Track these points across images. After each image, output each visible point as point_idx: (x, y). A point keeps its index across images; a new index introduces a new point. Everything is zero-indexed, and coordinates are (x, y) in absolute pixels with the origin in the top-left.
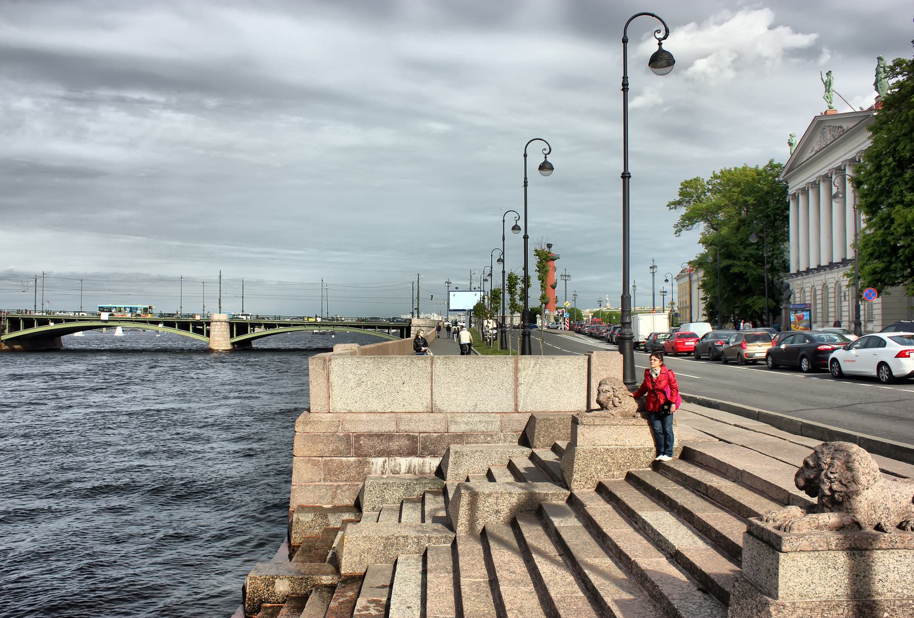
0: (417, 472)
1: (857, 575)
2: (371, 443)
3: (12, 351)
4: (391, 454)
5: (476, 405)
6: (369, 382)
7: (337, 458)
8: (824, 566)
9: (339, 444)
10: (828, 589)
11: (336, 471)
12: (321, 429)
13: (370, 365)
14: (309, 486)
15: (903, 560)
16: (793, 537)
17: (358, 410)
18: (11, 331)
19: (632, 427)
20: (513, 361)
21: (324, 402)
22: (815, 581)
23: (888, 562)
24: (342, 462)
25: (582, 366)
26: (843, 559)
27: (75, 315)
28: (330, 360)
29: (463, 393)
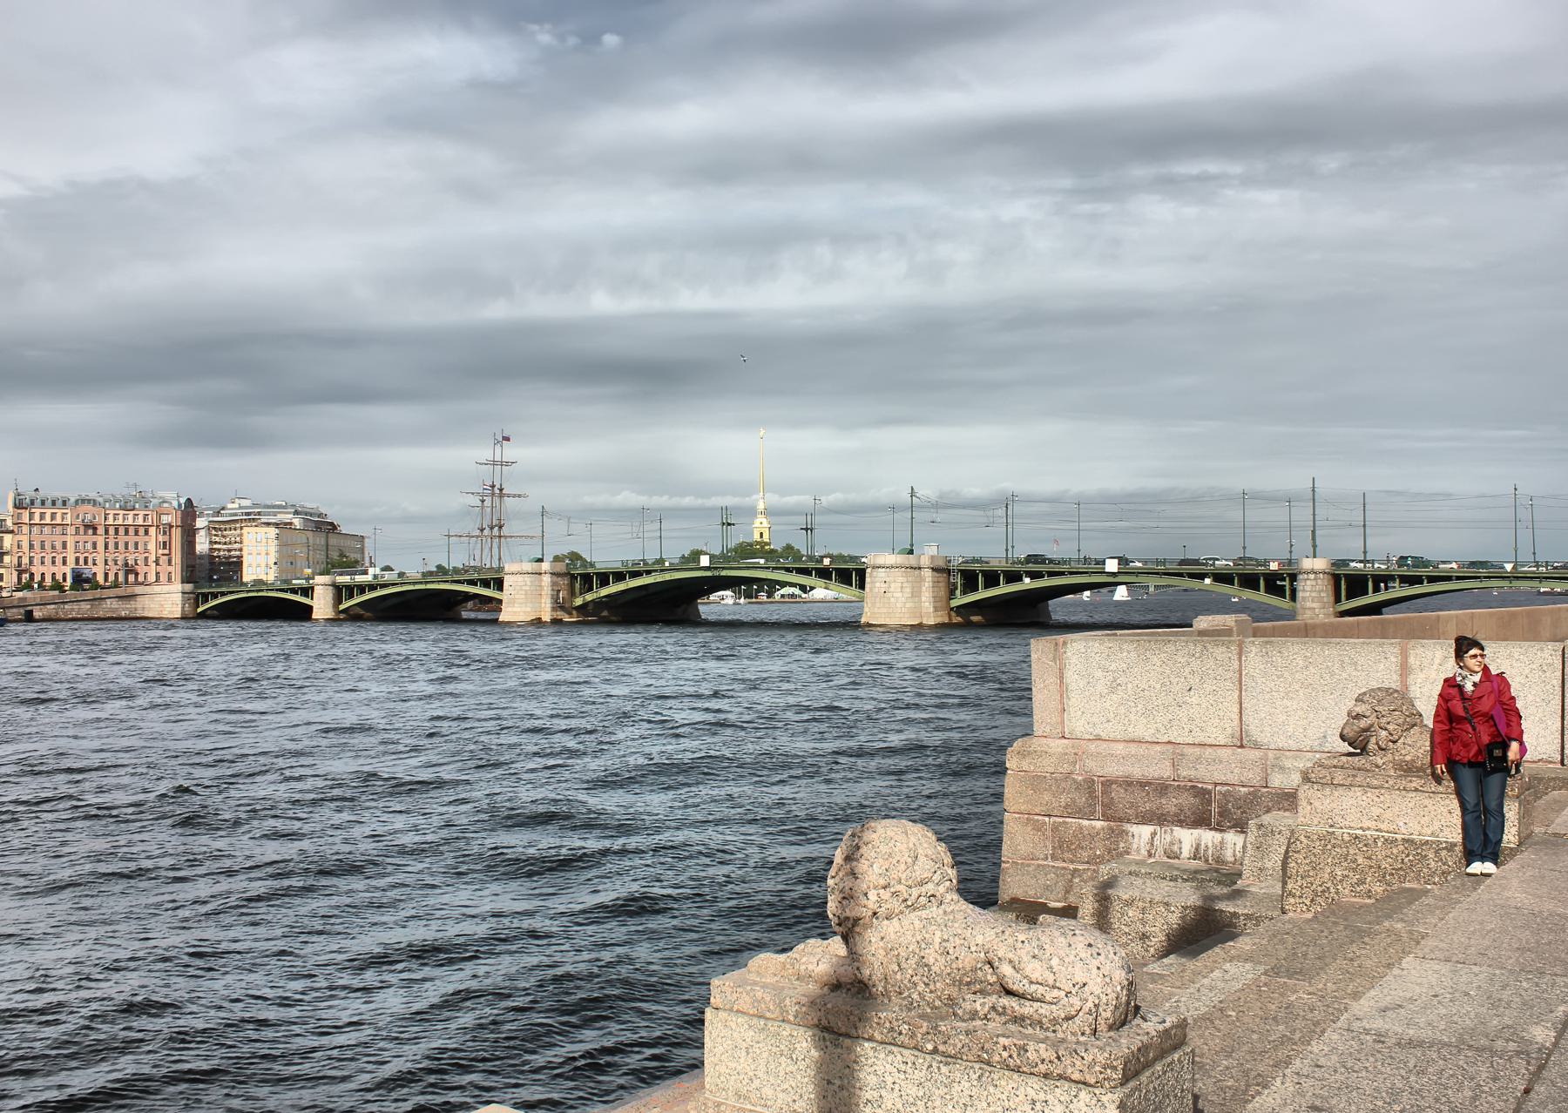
0: (1210, 858)
1: (829, 1082)
2: (1129, 798)
3: (967, 625)
4: (1165, 820)
5: (1325, 737)
6: (1130, 685)
7: (1074, 820)
8: (774, 1050)
9: (1076, 795)
10: (781, 1095)
11: (1072, 844)
12: (1047, 766)
13: (1132, 654)
14: (1029, 865)
15: (910, 1071)
16: (727, 984)
17: (1112, 736)
18: (964, 592)
19: (1414, 794)
20: (1397, 650)
21: (1055, 719)
22: (760, 1074)
23: (882, 1067)
24: (1082, 829)
25: (1550, 665)
26: (805, 1044)
27: (1365, 566)
28: (1065, 643)
29: (1300, 713)
